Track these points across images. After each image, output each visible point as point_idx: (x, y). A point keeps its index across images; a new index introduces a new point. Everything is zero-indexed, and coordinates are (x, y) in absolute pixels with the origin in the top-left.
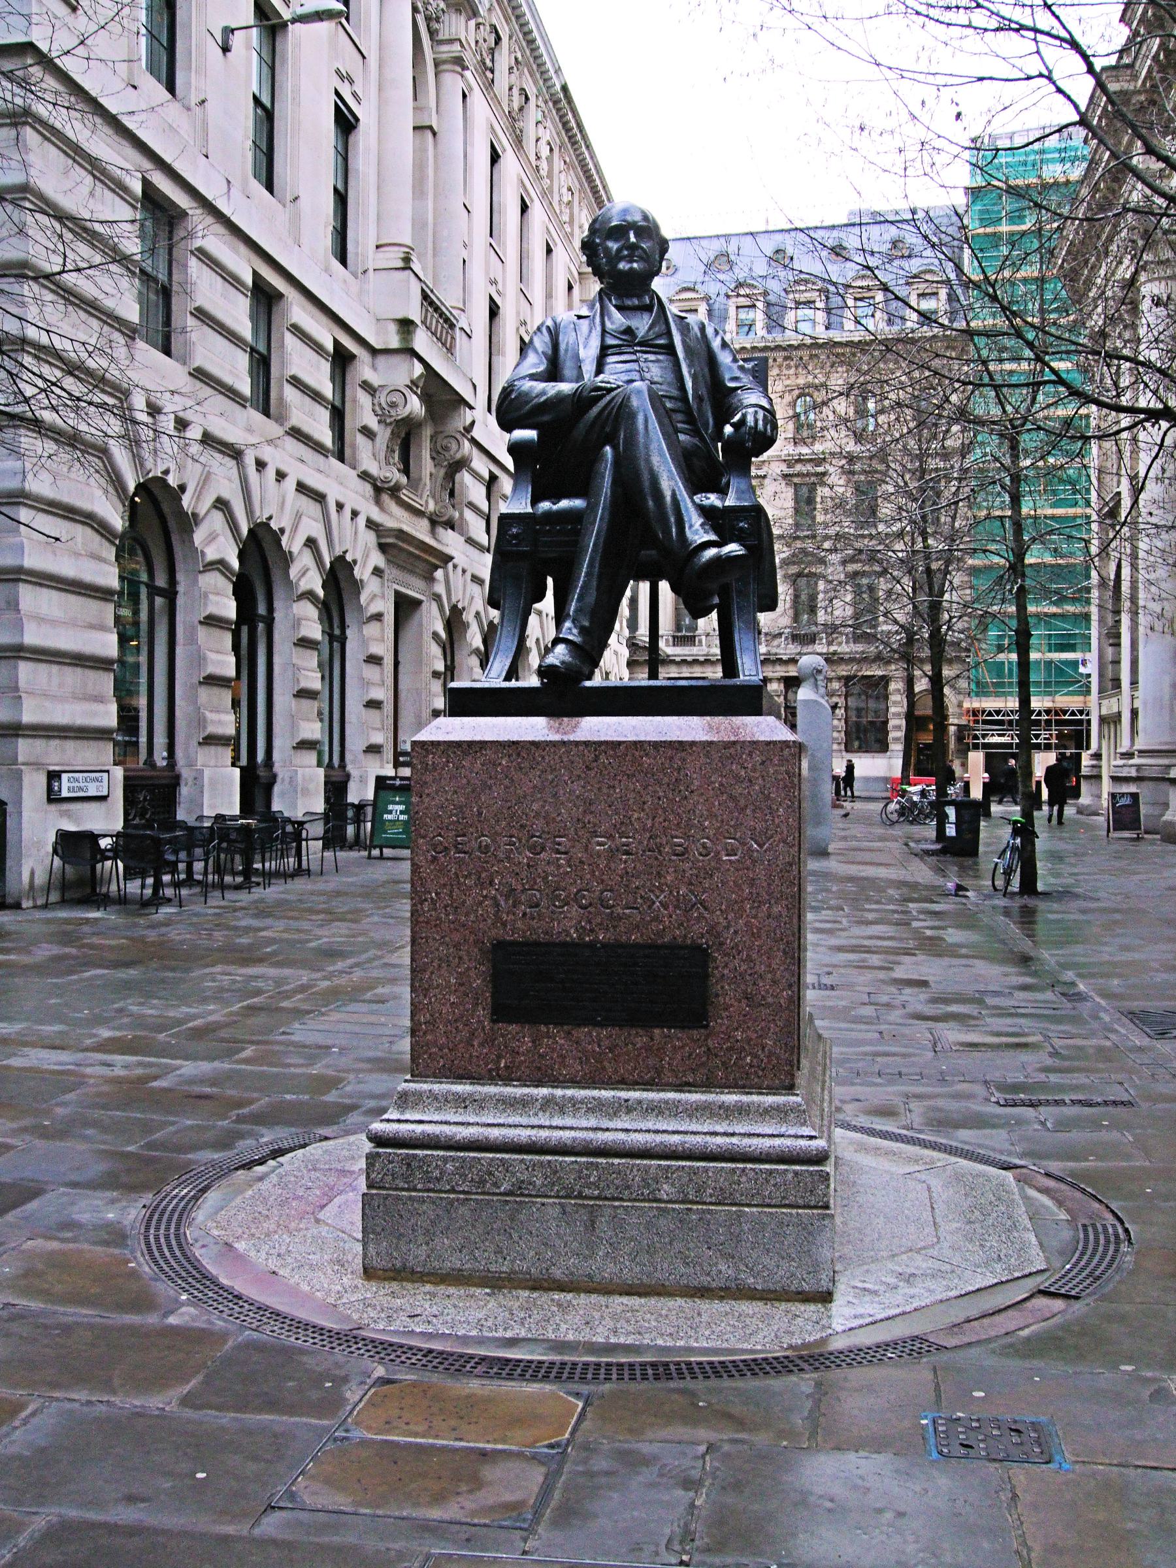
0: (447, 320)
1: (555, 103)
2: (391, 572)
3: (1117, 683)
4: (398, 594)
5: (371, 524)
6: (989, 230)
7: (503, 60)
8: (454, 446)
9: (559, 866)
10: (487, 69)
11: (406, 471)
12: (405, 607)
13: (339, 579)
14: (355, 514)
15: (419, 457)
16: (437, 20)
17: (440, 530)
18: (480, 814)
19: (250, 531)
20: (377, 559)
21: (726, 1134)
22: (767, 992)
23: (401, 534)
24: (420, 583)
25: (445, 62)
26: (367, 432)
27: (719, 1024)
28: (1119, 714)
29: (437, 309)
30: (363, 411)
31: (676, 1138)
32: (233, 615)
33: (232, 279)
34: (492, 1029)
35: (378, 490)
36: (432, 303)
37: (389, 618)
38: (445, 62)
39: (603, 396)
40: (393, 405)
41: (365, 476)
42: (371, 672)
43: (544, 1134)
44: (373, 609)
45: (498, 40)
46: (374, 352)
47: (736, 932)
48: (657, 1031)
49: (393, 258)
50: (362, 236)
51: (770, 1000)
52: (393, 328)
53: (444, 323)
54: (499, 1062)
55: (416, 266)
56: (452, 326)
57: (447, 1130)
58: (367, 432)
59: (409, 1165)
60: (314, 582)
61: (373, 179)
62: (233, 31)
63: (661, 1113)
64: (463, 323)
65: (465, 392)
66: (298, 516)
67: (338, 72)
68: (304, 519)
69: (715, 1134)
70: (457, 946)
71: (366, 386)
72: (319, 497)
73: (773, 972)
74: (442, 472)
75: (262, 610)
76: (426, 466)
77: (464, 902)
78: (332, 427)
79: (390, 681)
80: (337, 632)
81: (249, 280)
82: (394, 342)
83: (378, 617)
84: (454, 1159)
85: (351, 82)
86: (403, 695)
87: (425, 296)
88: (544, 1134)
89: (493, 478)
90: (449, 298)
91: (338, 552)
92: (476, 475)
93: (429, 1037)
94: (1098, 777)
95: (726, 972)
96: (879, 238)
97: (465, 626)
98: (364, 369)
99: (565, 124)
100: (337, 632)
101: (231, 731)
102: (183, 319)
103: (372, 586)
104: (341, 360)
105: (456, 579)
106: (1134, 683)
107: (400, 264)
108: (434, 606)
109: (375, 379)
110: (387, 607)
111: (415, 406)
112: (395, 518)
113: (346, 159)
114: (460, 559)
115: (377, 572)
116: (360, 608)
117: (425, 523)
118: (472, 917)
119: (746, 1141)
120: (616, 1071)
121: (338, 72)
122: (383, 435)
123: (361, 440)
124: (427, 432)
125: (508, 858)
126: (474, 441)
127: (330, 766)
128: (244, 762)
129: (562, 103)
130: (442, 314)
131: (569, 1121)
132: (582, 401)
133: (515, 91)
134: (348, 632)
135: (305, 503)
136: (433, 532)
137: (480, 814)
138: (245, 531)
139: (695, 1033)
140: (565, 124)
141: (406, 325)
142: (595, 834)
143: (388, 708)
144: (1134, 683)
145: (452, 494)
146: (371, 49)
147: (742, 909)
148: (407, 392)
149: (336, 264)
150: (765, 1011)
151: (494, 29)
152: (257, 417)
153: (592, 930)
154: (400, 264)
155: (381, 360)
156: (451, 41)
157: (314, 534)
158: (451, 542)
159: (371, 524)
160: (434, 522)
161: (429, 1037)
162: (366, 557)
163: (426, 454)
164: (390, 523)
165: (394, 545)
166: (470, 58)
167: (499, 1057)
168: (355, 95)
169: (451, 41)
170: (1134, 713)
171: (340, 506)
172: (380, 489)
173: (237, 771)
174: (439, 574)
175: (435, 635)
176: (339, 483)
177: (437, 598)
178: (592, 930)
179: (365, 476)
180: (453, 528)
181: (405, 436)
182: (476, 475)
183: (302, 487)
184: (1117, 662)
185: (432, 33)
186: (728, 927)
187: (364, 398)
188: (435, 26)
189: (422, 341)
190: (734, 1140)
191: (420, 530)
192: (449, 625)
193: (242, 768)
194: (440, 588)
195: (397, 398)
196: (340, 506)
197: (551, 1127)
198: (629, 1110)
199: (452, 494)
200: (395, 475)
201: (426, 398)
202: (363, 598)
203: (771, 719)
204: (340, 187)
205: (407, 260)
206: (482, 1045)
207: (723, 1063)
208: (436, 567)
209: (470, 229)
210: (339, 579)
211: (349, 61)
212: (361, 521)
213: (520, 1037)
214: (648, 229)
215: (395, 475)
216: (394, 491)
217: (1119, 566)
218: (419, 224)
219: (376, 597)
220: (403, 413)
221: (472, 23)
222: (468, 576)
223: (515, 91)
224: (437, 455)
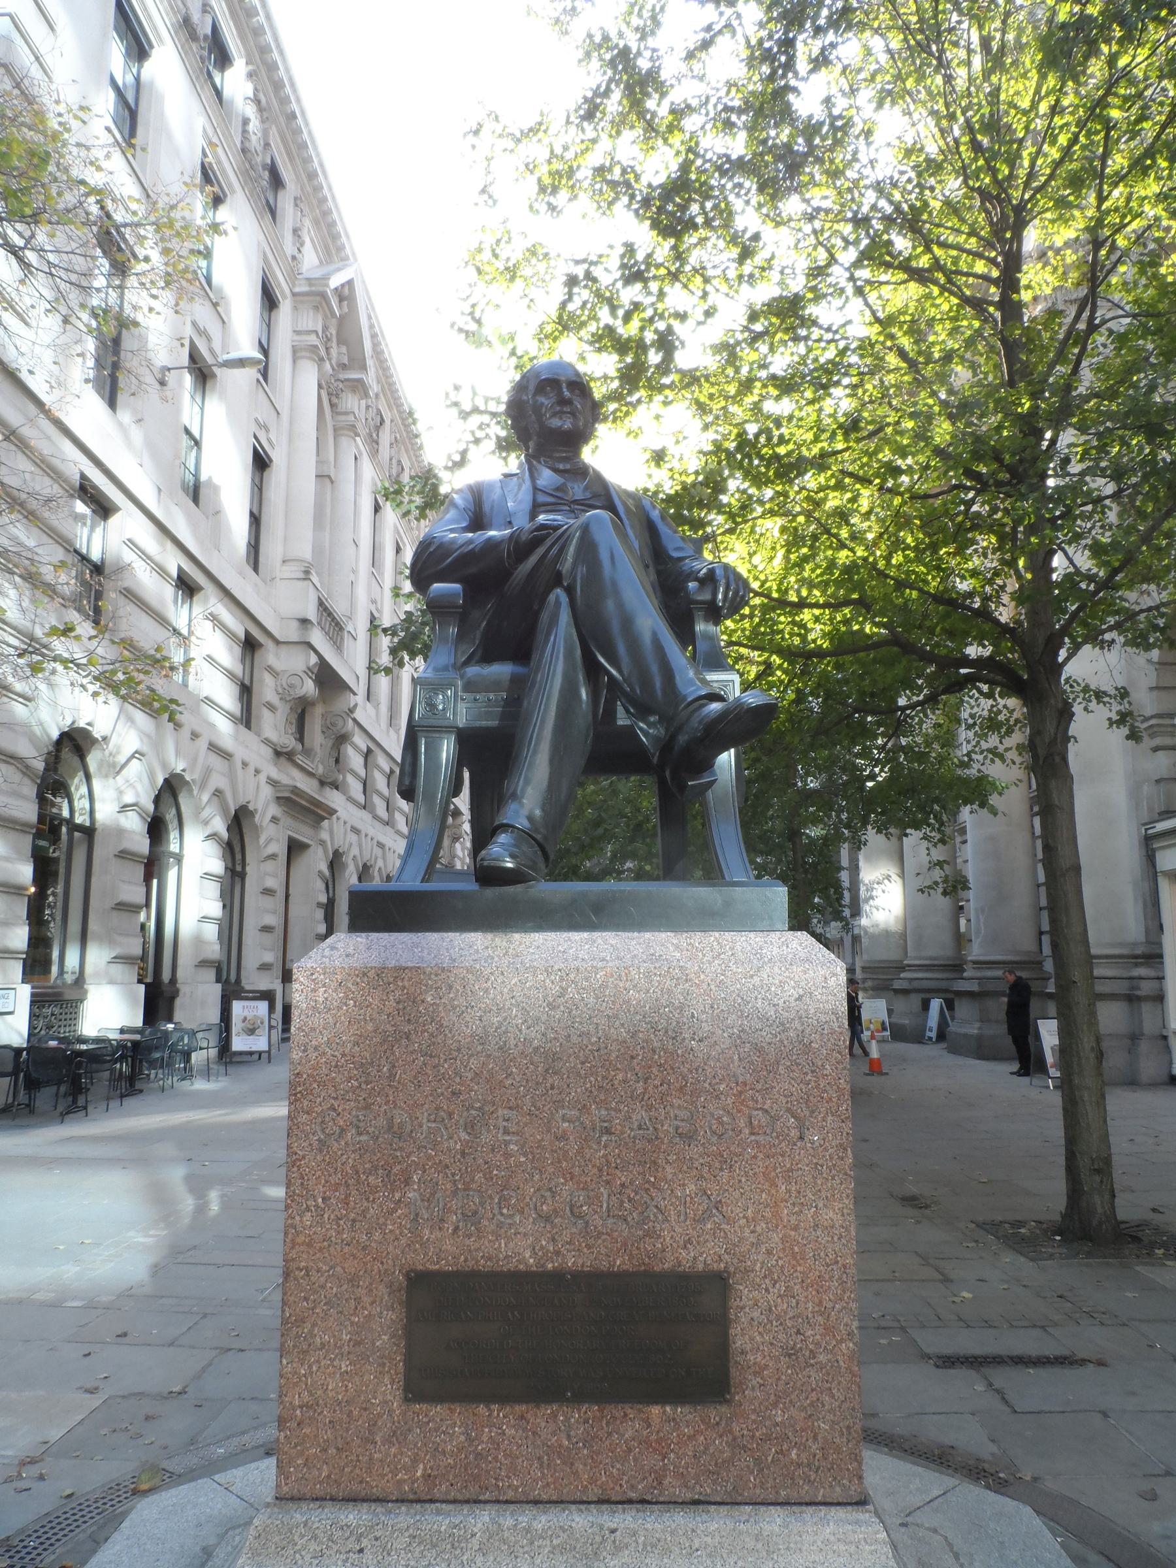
0: (337, 624)
2: (286, 821)
5: (273, 782)
7: (385, 437)
8: (340, 723)
9: (507, 1155)
10: (374, 443)
11: (301, 739)
12: (295, 848)
14: (257, 771)
16: (337, 396)
18: (391, 1076)
19: (166, 780)
20: (274, 810)
22: (818, 1344)
23: (295, 790)
25: (342, 428)
27: (750, 1392)
30: (267, 689)
33: (161, 571)
34: (404, 1414)
35: (278, 754)
36: (326, 609)
38: (342, 428)
39: (548, 535)
40: (291, 686)
41: (267, 742)
42: (268, 902)
45: (382, 421)
46: (277, 642)
47: (769, 1252)
48: (655, 1410)
49: (294, 570)
50: (272, 549)
51: (822, 1358)
52: (295, 624)
53: (334, 626)
54: (414, 1468)
55: (315, 578)
56: (341, 629)
58: (271, 707)
62: (169, 369)
64: (350, 628)
65: (351, 682)
66: (208, 772)
67: (256, 420)
70: (353, 1280)
71: (270, 669)
74: (330, 744)
76: (317, 737)
77: (365, 1211)
80: (239, 868)
82: (295, 638)
83: (273, 857)
85: (267, 431)
87: (321, 603)
89: (369, 751)
90: (339, 607)
92: (356, 747)
93: (307, 1430)
95: (756, 1314)
97: (344, 866)
98: (271, 656)
100: (239, 868)
101: (138, 951)
102: (111, 600)
105: (338, 829)
107: (302, 575)
108: (320, 851)
109: (278, 665)
110: (279, 848)
111: (309, 687)
113: (260, 490)
114: (342, 813)
115: (274, 820)
117: (315, 783)
118: (377, 1236)
120: (593, 1480)
121: (256, 420)
122: (283, 710)
123: (266, 713)
124: (319, 710)
125: (435, 1144)
126: (354, 720)
127: (227, 982)
130: (334, 619)
133: (394, 461)
134: (248, 869)
135: (215, 761)
137: (391, 1076)
139: (714, 1413)
141: (304, 622)
142: (559, 1104)
145: (337, 761)
146: (284, 406)
148: (304, 676)
149: (249, 571)
150: (815, 1376)
151: (379, 413)
153: (557, 1253)
154: (302, 575)
155: (284, 650)
156: (346, 413)
158: (334, 799)
159: (273, 782)
161: (307, 1430)
163: (318, 728)
164: (285, 780)
166: (360, 428)
167: (415, 1461)
168: (269, 440)
169: (346, 413)
173: (142, 987)
174: (326, 823)
177: (322, 843)
179: (267, 742)
180: (337, 788)
181: (301, 712)
182: (356, 747)
185: (332, 405)
186: (756, 1245)
187: (268, 679)
188: (335, 400)
189: (317, 638)
193: (148, 986)
194: (325, 835)
195: (295, 681)
196: (245, 764)
199: (337, 761)
200: (290, 742)
202: (262, 840)
204: (255, 511)
205: (307, 572)
206: (388, 1441)
207: (758, 1461)
208: (323, 818)
209: (357, 556)
211: (264, 413)
212: (262, 778)
213: (450, 1426)
215: (290, 742)
218: (318, 549)
219: (270, 837)
220: (300, 692)
221: (363, 402)
223: (394, 461)
224: (326, 729)
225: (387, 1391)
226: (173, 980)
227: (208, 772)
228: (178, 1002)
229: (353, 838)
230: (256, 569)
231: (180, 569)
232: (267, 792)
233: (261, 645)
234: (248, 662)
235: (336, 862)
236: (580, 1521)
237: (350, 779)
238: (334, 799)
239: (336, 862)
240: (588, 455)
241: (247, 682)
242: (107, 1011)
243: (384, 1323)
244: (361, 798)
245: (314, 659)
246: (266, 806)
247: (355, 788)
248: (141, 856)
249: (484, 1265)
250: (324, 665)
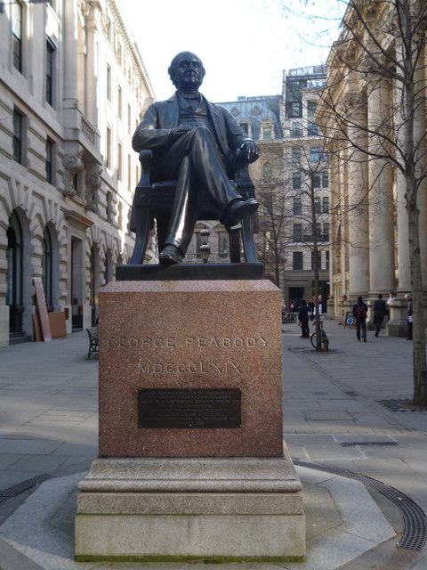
1: (131, 49)
2: (71, 228)
3: (339, 271)
4: (72, 236)
5: (62, 209)
6: (165, 184)
11: (76, 189)
12: (75, 242)
13: (49, 229)
14: (56, 205)
15: (81, 183)
17: (89, 212)
20: (64, 223)
21: (252, 480)
24: (81, 233)
26: (61, 173)
27: (248, 425)
28: (341, 282)
29: (87, 125)
30: (59, 164)
31: (229, 483)
32: (7, 244)
33: (40, 137)
37: (69, 246)
41: (59, 190)
43: (165, 483)
44: (63, 243)
46: (63, 140)
48: (218, 430)
57: (117, 483)
58: (61, 173)
59: (98, 501)
60: (39, 231)
61: (61, 71)
63: (221, 470)
66: (33, 205)
68: (36, 207)
69: (247, 480)
71: (60, 154)
72: (42, 198)
73: (272, 400)
75: (18, 241)
78: (47, 170)
79: (69, 271)
81: (13, 108)
82: (71, 137)
84: (121, 497)
86: (75, 276)
87: (83, 120)
88: (165, 483)
91: (49, 219)
94: (333, 305)
96: (250, 107)
99: (135, 58)
101: (6, 290)
103: (62, 233)
104: (50, 143)
106: (347, 270)
110: (67, 241)
111: (79, 162)
112: (70, 206)
113: (51, 62)
115: (65, 228)
116: (58, 242)
119: (262, 483)
124: (84, 173)
128: (11, 303)
129: (133, 50)
131: (176, 476)
132: (172, 138)
134: (53, 251)
135: (36, 200)
136: (85, 213)
138: (11, 210)
139: (236, 430)
140: (135, 58)
143: (69, 281)
144: (347, 270)
147: (257, 370)
152: (16, 164)
153: (186, 383)
157: (39, 212)
158: (92, 216)
159: (62, 209)
160: (87, 209)
162: (60, 223)
163: (83, 182)
164: (69, 209)
165: (69, 216)
170: (347, 282)
171: (50, 201)
172: (65, 195)
173: (8, 307)
174: (88, 229)
175: (87, 253)
176: (51, 193)
177: (88, 238)
178: (186, 383)
181: (75, 176)
183: (35, 193)
184: (339, 263)
189: (82, 138)
190: (257, 483)
191: (80, 210)
192: (92, 250)
194: (89, 235)
196: (50, 201)
197: (169, 480)
198: (206, 469)
201: (84, 160)
203: (268, 281)
210: (49, 229)
213: (153, 436)
214: (198, 64)
216: (71, 197)
217: (340, 229)
219: (64, 237)
222: (30, 193)
224: (88, 182)
225: (134, 424)
226: (21, 304)
227: (33, 205)
228: (24, 313)
229: (102, 235)
230: (50, 103)
231: (48, 136)
232: (60, 214)
233: (55, 142)
234: (18, 124)
235: (94, 249)
236: (194, 462)
237: (99, 206)
238: (92, 216)
239: (94, 249)
240: (201, 90)
241: (18, 136)
242: (153, 258)
243: (132, 407)
244: (106, 216)
245: (81, 148)
246: (60, 221)
247: (103, 211)
248: (4, 246)
249: (163, 387)
250: (86, 150)
